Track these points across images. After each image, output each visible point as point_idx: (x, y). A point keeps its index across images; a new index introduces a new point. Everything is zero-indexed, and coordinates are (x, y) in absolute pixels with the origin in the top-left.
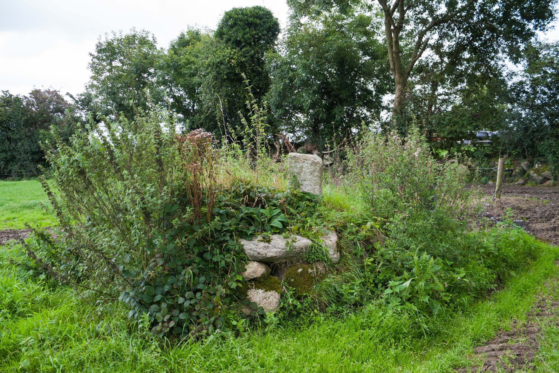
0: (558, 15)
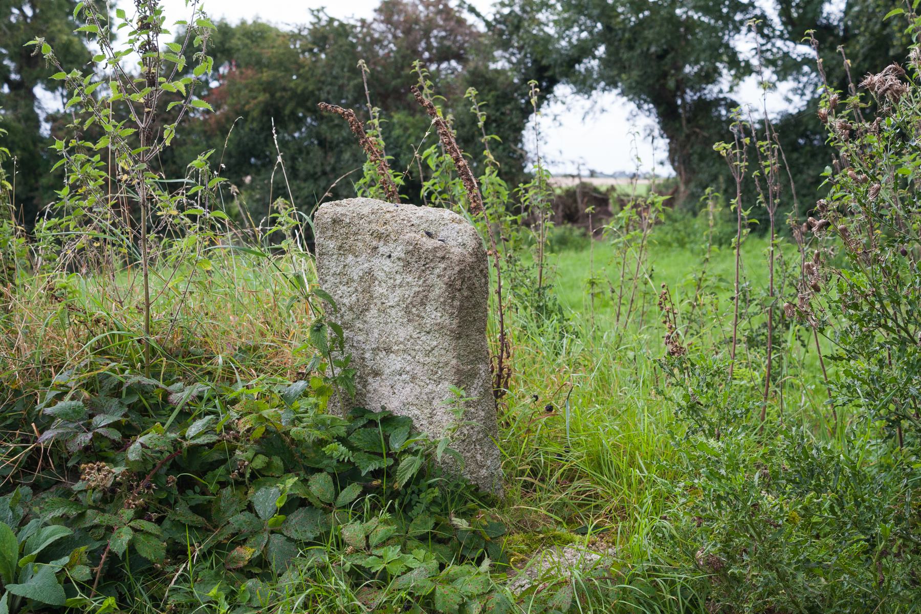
0: (240, 17)
